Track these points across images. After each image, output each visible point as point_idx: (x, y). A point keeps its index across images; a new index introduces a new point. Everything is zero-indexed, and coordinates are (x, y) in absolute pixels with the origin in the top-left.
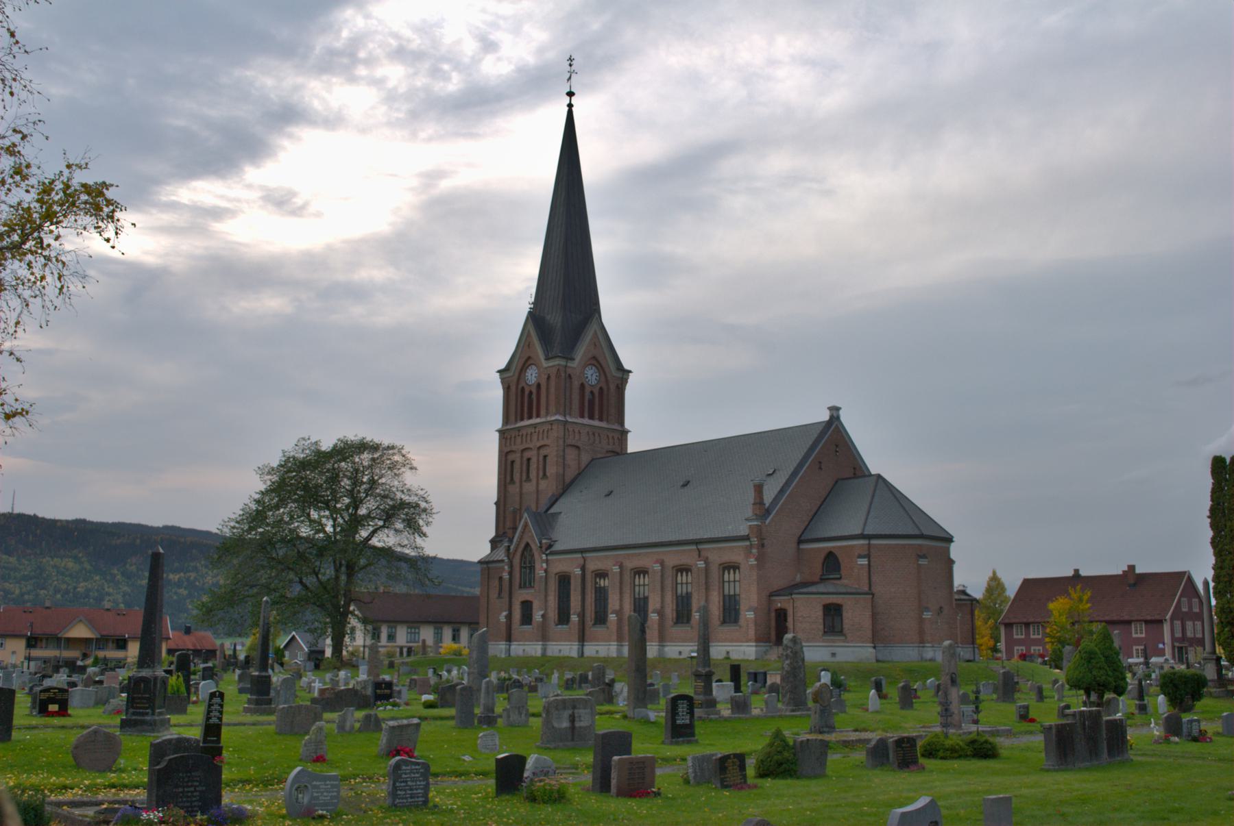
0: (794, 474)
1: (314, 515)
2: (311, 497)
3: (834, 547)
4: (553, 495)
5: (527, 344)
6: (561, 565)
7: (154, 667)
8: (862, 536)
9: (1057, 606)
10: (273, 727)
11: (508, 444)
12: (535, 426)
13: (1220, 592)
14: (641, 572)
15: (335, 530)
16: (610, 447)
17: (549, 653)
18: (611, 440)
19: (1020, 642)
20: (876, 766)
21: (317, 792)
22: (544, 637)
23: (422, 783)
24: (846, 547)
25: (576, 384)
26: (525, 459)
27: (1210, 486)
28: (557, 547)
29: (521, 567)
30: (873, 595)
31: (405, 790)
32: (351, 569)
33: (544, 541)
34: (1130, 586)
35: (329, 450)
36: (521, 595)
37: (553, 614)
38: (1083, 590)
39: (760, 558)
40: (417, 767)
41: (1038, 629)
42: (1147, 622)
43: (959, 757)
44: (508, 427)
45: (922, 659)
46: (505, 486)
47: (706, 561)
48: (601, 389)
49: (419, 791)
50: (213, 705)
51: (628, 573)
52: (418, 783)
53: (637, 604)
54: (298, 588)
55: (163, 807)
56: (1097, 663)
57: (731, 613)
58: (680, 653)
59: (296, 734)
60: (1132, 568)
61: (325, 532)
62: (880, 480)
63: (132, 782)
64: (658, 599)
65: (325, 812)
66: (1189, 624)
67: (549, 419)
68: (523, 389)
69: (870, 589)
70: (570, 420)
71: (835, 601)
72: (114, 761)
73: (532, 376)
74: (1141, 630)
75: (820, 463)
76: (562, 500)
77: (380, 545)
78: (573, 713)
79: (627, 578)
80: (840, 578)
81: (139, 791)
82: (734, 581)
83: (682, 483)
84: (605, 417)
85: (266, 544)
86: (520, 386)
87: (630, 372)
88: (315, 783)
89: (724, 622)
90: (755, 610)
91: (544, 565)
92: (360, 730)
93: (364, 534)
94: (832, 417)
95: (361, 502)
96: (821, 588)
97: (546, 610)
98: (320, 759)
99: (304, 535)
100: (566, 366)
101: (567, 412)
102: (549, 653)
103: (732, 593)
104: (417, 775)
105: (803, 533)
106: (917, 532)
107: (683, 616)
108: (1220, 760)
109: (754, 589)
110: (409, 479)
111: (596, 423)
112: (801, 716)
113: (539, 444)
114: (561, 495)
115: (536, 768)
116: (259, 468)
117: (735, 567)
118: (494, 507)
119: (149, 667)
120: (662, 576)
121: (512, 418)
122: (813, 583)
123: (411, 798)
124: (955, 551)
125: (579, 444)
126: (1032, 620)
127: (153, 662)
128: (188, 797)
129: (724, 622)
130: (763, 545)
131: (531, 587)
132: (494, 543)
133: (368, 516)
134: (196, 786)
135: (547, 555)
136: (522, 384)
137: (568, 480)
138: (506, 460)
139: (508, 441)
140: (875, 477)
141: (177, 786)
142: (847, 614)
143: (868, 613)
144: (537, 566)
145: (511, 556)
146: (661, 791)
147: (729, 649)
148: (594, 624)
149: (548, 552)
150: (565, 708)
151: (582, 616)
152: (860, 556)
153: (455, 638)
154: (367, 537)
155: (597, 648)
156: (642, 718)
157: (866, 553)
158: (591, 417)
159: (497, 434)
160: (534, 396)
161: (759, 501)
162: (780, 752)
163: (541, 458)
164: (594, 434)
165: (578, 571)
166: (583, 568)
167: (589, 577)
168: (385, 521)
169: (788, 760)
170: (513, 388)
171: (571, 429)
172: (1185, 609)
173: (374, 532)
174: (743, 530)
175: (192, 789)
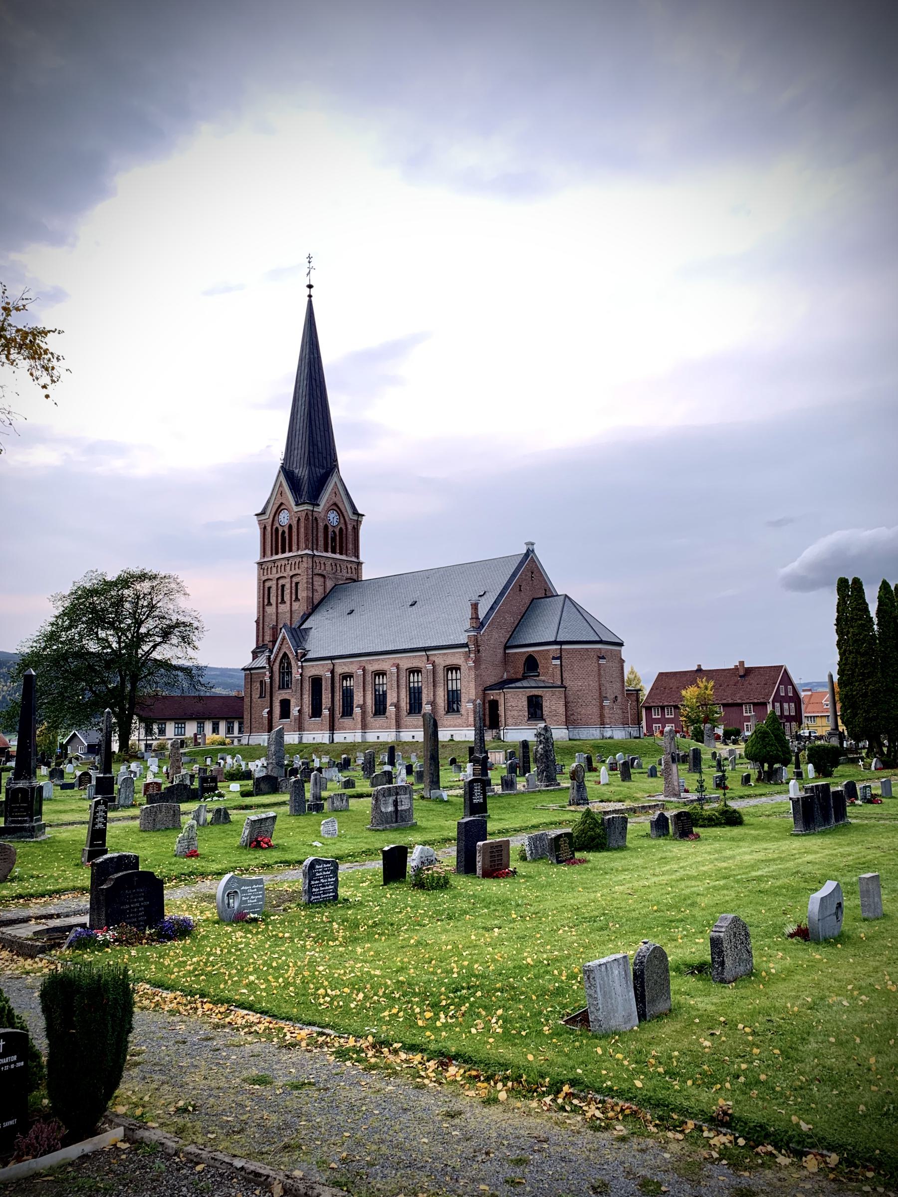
0: (502, 594)
1: (102, 634)
2: (98, 619)
3: (533, 651)
4: (304, 614)
5: (280, 492)
6: (313, 670)
7: (30, 779)
8: (555, 643)
9: (690, 693)
10: (137, 822)
11: (265, 574)
12: (288, 559)
13: (844, 682)
14: (381, 673)
15: (120, 646)
16: (349, 575)
17: (304, 741)
18: (349, 571)
19: (657, 721)
20: (660, 836)
21: (245, 896)
22: (300, 728)
23: (333, 879)
24: (543, 651)
25: (321, 525)
26: (280, 585)
27: (837, 601)
28: (309, 656)
29: (280, 672)
30: (565, 688)
31: (319, 887)
32: (135, 679)
33: (299, 651)
34: (741, 676)
35: (114, 580)
36: (280, 695)
37: (307, 709)
38: (708, 681)
39: (477, 661)
40: (328, 865)
41: (671, 711)
42: (755, 704)
43: (716, 825)
44: (266, 560)
45: (603, 738)
46: (264, 608)
47: (433, 664)
48: (341, 529)
49: (330, 887)
50: (98, 812)
51: (370, 675)
52: (329, 880)
53: (378, 699)
54: (88, 694)
55: (114, 926)
56: (770, 741)
57: (453, 702)
58: (413, 737)
59: (159, 830)
60: (742, 663)
61: (112, 648)
62: (567, 599)
63: (37, 891)
64: (395, 695)
65: (256, 915)
66: (786, 706)
67: (300, 553)
68: (277, 529)
69: (562, 683)
70: (316, 554)
71: (536, 693)
72: (10, 871)
73: (284, 518)
74: (750, 710)
75: (520, 586)
76: (311, 618)
77: (159, 658)
78: (396, 798)
79: (369, 678)
80: (538, 676)
81: (45, 899)
82: (456, 679)
83: (410, 603)
84: (344, 552)
85: (58, 659)
86: (274, 527)
87: (363, 515)
88: (243, 888)
89: (448, 712)
90: (474, 702)
91: (300, 670)
92: (211, 823)
93: (146, 648)
94: (528, 551)
95: (142, 622)
96: (525, 683)
97: (302, 706)
98: (193, 854)
99: (93, 650)
100: (313, 511)
101: (315, 547)
102: (304, 741)
103: (455, 688)
104: (328, 873)
105: (508, 640)
106: (598, 639)
107: (415, 706)
108: (764, 795)
109: (472, 685)
110: (182, 602)
111: (338, 556)
112: (553, 790)
113: (291, 574)
114: (309, 615)
115: (422, 857)
116: (52, 596)
117: (457, 668)
118: (255, 624)
119: (25, 778)
120: (398, 676)
121: (268, 552)
122: (518, 680)
123: (324, 894)
124: (625, 653)
125: (324, 573)
126: (666, 704)
127: (30, 775)
128: (134, 913)
129: (448, 712)
130: (479, 651)
131: (288, 687)
132: (255, 654)
133: (147, 634)
134: (140, 902)
135: (302, 662)
136: (276, 525)
137: (316, 602)
138: (264, 586)
139: (265, 571)
140: (563, 597)
141: (124, 904)
142: (546, 705)
143: (562, 703)
144: (294, 671)
145: (272, 663)
146: (517, 870)
147: (452, 733)
148: (341, 717)
149: (303, 660)
150: (390, 795)
151: (332, 710)
152: (554, 658)
153: (215, 730)
154: (148, 651)
155: (345, 735)
156: (437, 798)
157: (559, 655)
158: (334, 552)
159: (256, 565)
160: (287, 535)
161: (475, 617)
162: (593, 829)
163: (294, 585)
164: (336, 565)
165: (329, 675)
166: (332, 672)
167: (337, 678)
168: (163, 637)
169: (600, 836)
170: (269, 528)
171: (317, 561)
172: (783, 694)
173: (154, 647)
174: (463, 639)
175: (137, 905)
